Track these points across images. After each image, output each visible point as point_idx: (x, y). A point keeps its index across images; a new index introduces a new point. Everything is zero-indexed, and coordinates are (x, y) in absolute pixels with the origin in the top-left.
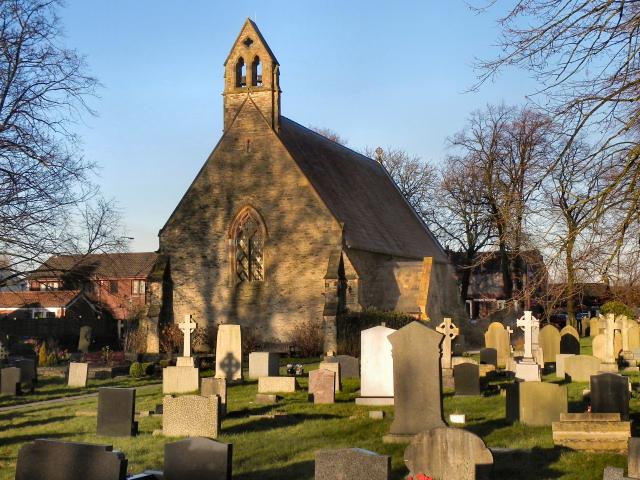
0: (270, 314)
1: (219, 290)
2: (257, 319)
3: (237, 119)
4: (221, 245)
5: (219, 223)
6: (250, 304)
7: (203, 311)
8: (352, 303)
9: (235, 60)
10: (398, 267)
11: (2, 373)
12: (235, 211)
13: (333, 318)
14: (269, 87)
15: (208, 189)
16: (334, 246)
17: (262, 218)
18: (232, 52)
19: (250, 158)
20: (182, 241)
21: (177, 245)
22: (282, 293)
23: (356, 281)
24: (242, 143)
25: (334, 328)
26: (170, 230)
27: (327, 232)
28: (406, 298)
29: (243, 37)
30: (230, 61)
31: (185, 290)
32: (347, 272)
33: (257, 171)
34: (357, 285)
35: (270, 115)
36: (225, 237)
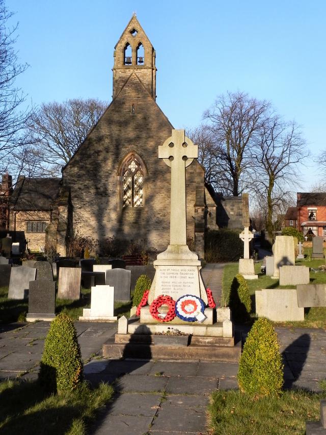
0: (149, 231)
1: (109, 214)
2: (138, 235)
3: (125, 88)
4: (111, 180)
6: (133, 223)
7: (96, 228)
8: (211, 224)
9: (123, 44)
10: (153, 204)
12: (122, 155)
13: (202, 234)
14: (150, 66)
15: (100, 139)
16: (198, 183)
17: (144, 162)
18: (121, 38)
19: (133, 117)
20: (79, 176)
21: (76, 179)
22: (159, 216)
23: (215, 208)
24: (128, 105)
25: (202, 241)
26: (71, 168)
27: (193, 173)
28: (234, 221)
29: (130, 28)
30: (119, 45)
31: (82, 212)
32: (208, 202)
33: (138, 127)
35: (150, 87)
36: (114, 174)
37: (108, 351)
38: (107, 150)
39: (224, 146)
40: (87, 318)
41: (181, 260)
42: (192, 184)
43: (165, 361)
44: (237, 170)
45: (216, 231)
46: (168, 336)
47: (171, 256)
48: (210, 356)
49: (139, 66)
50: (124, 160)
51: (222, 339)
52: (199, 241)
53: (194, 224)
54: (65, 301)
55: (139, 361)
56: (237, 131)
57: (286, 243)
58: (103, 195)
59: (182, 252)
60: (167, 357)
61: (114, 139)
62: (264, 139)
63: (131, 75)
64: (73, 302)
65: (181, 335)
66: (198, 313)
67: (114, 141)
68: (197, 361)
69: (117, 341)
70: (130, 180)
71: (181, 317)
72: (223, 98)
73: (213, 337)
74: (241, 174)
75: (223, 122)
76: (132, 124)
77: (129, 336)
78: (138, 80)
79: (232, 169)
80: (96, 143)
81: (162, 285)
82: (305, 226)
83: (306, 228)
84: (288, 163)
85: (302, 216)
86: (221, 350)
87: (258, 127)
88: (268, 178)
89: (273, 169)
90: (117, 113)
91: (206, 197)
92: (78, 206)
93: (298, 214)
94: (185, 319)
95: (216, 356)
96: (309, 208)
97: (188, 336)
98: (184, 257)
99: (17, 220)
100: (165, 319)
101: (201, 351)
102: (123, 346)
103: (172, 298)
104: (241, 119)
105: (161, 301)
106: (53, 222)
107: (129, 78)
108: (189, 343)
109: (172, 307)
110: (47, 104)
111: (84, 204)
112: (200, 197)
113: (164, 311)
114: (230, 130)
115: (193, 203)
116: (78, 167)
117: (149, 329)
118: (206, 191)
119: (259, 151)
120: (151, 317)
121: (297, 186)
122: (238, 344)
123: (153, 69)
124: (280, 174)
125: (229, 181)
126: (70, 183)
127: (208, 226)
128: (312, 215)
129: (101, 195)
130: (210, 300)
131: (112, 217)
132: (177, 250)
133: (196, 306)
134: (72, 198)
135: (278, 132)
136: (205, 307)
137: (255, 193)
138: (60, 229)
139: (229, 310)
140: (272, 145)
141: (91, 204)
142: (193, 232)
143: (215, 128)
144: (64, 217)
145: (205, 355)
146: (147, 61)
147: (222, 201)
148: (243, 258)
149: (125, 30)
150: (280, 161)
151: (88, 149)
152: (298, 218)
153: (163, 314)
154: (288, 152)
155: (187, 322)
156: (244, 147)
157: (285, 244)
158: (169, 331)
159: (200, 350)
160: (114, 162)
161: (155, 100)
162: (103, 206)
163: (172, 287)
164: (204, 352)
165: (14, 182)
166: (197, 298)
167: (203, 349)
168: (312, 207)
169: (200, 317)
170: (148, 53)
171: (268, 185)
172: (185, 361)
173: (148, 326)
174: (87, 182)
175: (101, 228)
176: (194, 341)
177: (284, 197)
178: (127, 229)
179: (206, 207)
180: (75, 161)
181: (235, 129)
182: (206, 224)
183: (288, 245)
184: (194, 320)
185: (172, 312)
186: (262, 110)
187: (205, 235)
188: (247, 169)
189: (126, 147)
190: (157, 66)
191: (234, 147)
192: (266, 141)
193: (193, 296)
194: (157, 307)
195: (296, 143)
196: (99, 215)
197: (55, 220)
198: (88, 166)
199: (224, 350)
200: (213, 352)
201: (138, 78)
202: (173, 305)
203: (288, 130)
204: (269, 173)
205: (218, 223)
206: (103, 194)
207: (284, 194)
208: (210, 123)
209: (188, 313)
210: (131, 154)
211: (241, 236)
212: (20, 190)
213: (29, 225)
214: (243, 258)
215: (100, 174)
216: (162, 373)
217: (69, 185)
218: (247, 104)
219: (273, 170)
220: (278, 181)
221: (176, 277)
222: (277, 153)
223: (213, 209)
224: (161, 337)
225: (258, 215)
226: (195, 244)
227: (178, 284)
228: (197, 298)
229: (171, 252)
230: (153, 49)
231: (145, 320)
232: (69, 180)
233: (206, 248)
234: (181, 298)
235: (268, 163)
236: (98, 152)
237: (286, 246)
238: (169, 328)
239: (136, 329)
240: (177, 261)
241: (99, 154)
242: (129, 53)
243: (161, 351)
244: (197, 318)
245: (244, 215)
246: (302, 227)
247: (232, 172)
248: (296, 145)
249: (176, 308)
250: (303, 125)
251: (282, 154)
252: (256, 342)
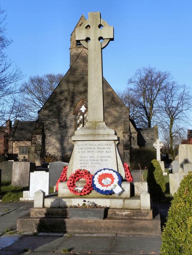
3: (77, 60)
4: (69, 117)
5: (67, 109)
11: (191, 169)
12: (76, 102)
13: (128, 151)
15: (62, 93)
16: (125, 118)
21: (47, 118)
23: (136, 134)
25: (129, 156)
26: (44, 110)
27: (122, 112)
31: (51, 139)
32: (132, 131)
34: (137, 137)
37: (22, 224)
38: (66, 99)
39: (142, 100)
40: (26, 199)
41: (98, 135)
42: (121, 120)
43: (80, 235)
44: (150, 115)
45: (138, 149)
48: (128, 229)
50: (78, 105)
51: (140, 212)
52: (127, 155)
53: (123, 145)
54: (16, 187)
55: (53, 236)
56: (149, 91)
57: (187, 149)
58: (65, 127)
59: (99, 128)
60: (82, 231)
61: (71, 92)
62: (166, 96)
63: (82, 51)
64: (22, 188)
65: (97, 207)
66: (115, 186)
67: (71, 93)
68: (114, 235)
69: (32, 215)
70: (81, 117)
71: (98, 190)
72: (140, 71)
73: (130, 209)
74: (153, 117)
75: (140, 86)
76: (82, 82)
77: (44, 210)
78: (86, 55)
79: (147, 114)
80: (60, 95)
81: (80, 160)
84: (182, 111)
86: (139, 223)
87: (162, 88)
88: (170, 120)
89: (172, 114)
90: (73, 76)
91: (131, 127)
92: (48, 134)
94: (102, 192)
95: (134, 229)
97: (104, 209)
98: (101, 132)
99: (13, 147)
100: (81, 192)
101: (118, 224)
102: (38, 220)
103: (89, 173)
105: (78, 175)
106: (33, 145)
107: (80, 54)
108: (105, 216)
109: (89, 180)
110: (33, 77)
111: (53, 134)
112: (127, 127)
113: (82, 184)
114: (145, 90)
115: (122, 131)
116: (48, 110)
117: (65, 202)
118: (131, 124)
119: (163, 103)
120: (69, 191)
121: (188, 125)
122: (156, 217)
124: (176, 117)
125: (145, 122)
126: (43, 120)
129: (63, 127)
130: (127, 174)
132: (95, 126)
133: (113, 179)
134: (45, 130)
135: (175, 91)
136: (122, 180)
137: (162, 129)
138: (37, 149)
139: (147, 184)
140: (171, 99)
141: (56, 133)
143: (136, 90)
144: (39, 142)
145: (122, 229)
147: (141, 131)
149: (77, 24)
150: (177, 108)
151: (54, 99)
153: (80, 188)
154: (181, 104)
155: (102, 195)
157: (186, 150)
158: (84, 204)
159: (116, 223)
160: (71, 106)
162: (64, 135)
163: (89, 162)
164: (122, 225)
165: (13, 123)
166: (114, 171)
167: (119, 222)
169: (117, 190)
171: (170, 124)
172: (101, 235)
173: (64, 200)
174: (54, 119)
176: (111, 214)
177: (180, 131)
179: (131, 134)
180: (47, 106)
181: (148, 90)
182: (131, 144)
183: (189, 152)
184: (111, 193)
185: (89, 185)
186: (165, 78)
187: (130, 151)
189: (78, 97)
191: (148, 102)
193: (110, 170)
194: (74, 181)
195: (186, 98)
197: (34, 144)
198: (55, 109)
199: (143, 223)
200: (131, 225)
202: (90, 179)
203: (181, 90)
205: (139, 144)
207: (180, 129)
208: (132, 86)
209: (105, 186)
210: (81, 101)
211: (154, 145)
212: (16, 128)
213: (21, 150)
215: (62, 114)
216: (70, 250)
217: (43, 122)
218: (155, 75)
221: (93, 152)
222: (175, 104)
223: (135, 135)
224: (76, 210)
226: (124, 158)
227: (96, 159)
228: (114, 171)
229: (89, 128)
231: (62, 194)
232: (43, 118)
233: (131, 161)
234: (98, 171)
236: (61, 101)
237: (187, 151)
238: (85, 201)
239: (52, 203)
240: (94, 137)
241: (62, 101)
243: (76, 225)
244: (114, 190)
247: (147, 116)
248: (187, 99)
249: (93, 181)
251: (178, 105)
252: (188, 205)
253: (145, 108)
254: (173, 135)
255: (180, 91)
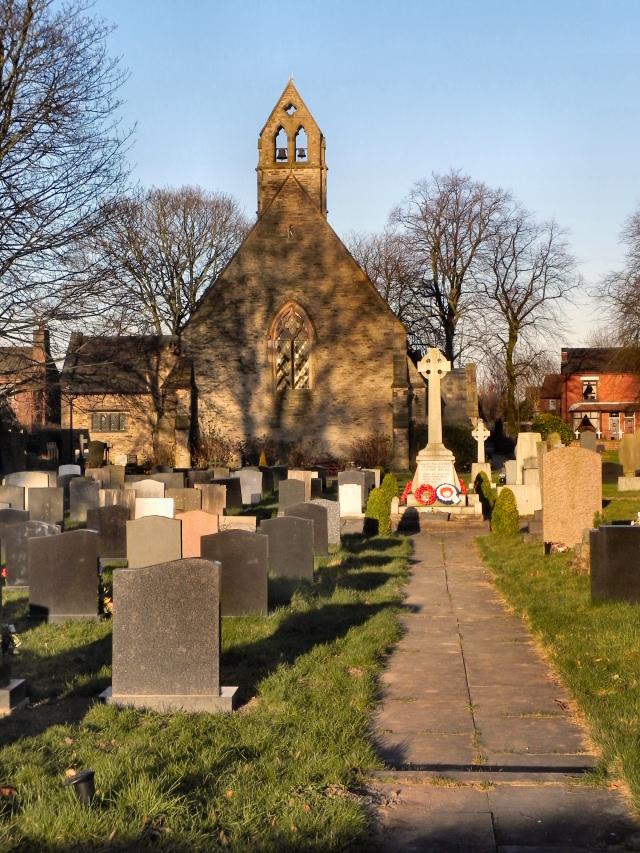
9: (274, 128)
14: (318, 163)
15: (242, 280)
25: (406, 442)
29: (285, 102)
46: (433, 514)
47: (429, 453)
49: (299, 163)
62: (499, 257)
71: (441, 501)
74: (460, 321)
77: (400, 516)
82: (577, 411)
83: (578, 415)
84: (543, 299)
85: (571, 391)
88: (508, 326)
93: (563, 389)
94: (444, 502)
96: (583, 378)
98: (441, 453)
104: (456, 219)
105: (423, 488)
107: (284, 183)
108: (449, 519)
115: (390, 382)
119: (491, 279)
123: (322, 169)
124: (528, 318)
127: (414, 418)
128: (589, 390)
131: (263, 401)
132: (435, 448)
133: (452, 492)
136: (459, 493)
140: (513, 265)
142: (391, 427)
146: (312, 156)
148: (476, 461)
149: (277, 105)
150: (529, 294)
152: (564, 396)
153: (425, 498)
154: (542, 278)
156: (463, 274)
161: (326, 218)
168: (590, 374)
169: (456, 499)
170: (315, 142)
171: (507, 340)
175: (248, 422)
178: (289, 421)
182: (410, 414)
184: (451, 503)
186: (496, 206)
188: (471, 313)
190: (328, 161)
191: (445, 273)
192: (502, 259)
196: (244, 402)
201: (299, 183)
203: (543, 239)
204: (508, 318)
206: (248, 369)
208: (401, 229)
211: (474, 434)
214: (476, 461)
219: (515, 311)
220: (527, 330)
225: (487, 390)
229: (428, 450)
230: (322, 136)
235: (507, 299)
240: (436, 456)
242: (282, 142)
243: (427, 526)
245: (468, 399)
246: (572, 412)
247: (443, 318)
248: (557, 267)
250: (569, 229)
253: (437, 295)
254: (516, 371)
255: (536, 244)
